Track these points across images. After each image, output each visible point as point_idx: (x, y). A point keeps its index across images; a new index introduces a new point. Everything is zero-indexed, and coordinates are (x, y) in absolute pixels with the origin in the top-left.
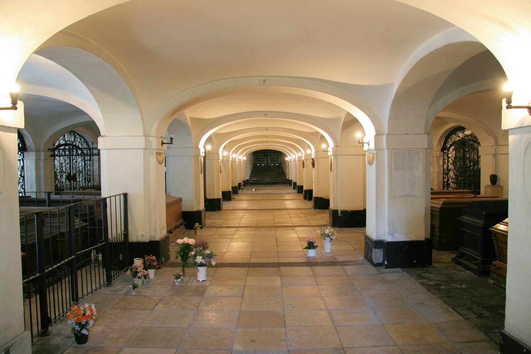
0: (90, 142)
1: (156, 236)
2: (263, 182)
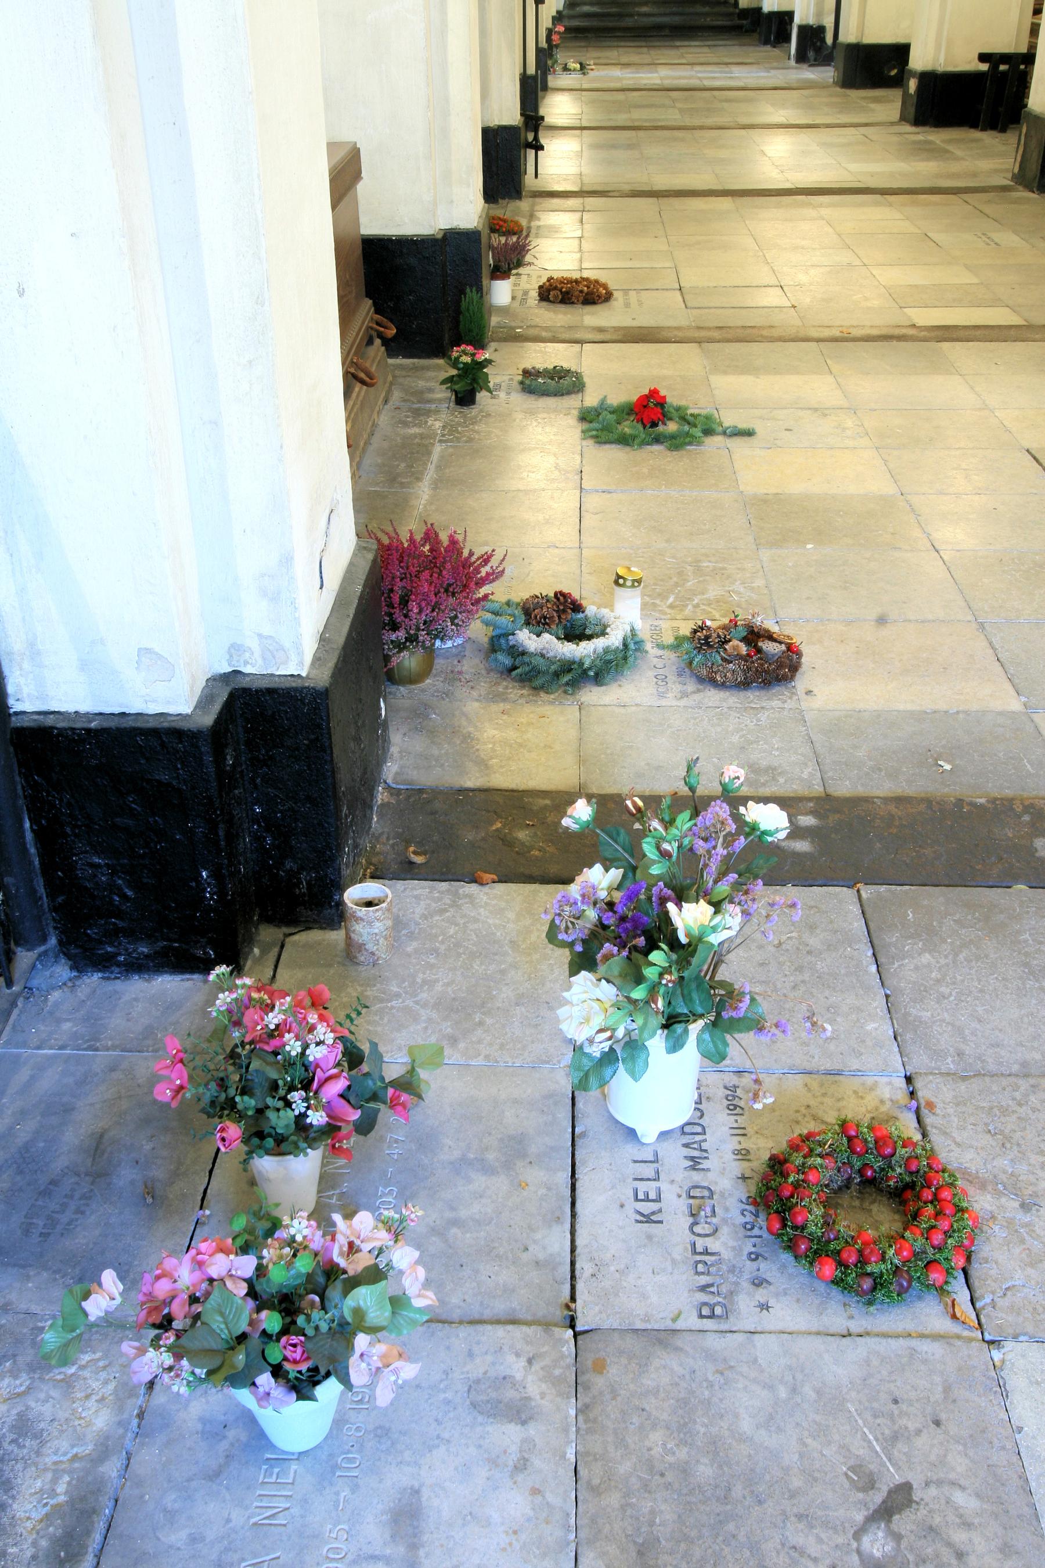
0: (737, 1527)
1: (365, 1048)
2: (629, 22)
